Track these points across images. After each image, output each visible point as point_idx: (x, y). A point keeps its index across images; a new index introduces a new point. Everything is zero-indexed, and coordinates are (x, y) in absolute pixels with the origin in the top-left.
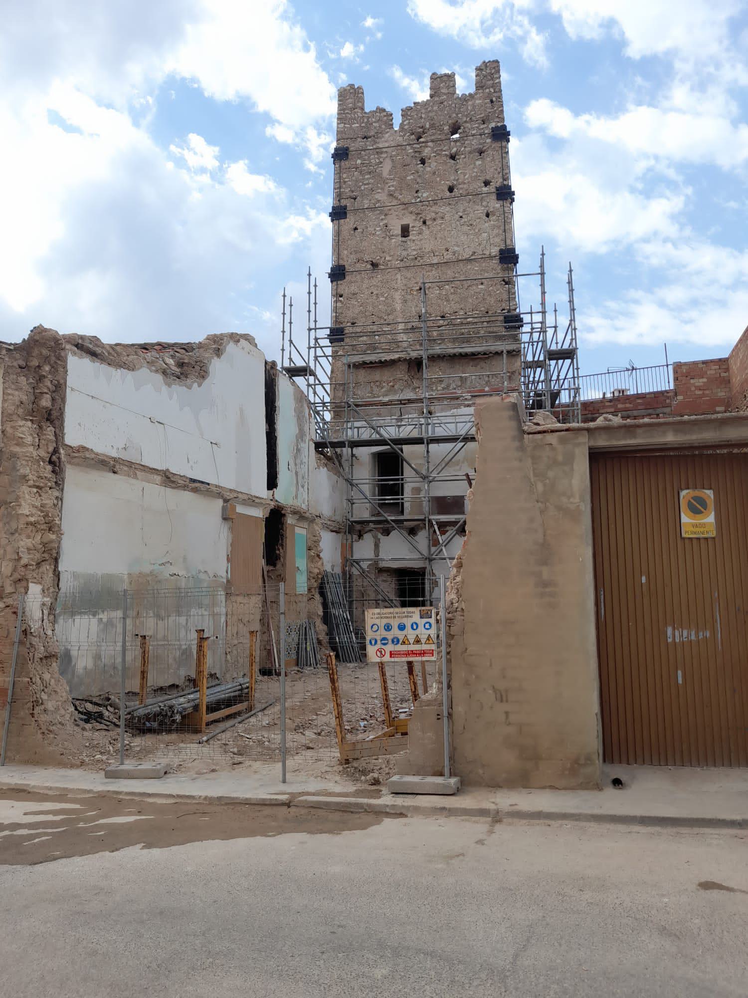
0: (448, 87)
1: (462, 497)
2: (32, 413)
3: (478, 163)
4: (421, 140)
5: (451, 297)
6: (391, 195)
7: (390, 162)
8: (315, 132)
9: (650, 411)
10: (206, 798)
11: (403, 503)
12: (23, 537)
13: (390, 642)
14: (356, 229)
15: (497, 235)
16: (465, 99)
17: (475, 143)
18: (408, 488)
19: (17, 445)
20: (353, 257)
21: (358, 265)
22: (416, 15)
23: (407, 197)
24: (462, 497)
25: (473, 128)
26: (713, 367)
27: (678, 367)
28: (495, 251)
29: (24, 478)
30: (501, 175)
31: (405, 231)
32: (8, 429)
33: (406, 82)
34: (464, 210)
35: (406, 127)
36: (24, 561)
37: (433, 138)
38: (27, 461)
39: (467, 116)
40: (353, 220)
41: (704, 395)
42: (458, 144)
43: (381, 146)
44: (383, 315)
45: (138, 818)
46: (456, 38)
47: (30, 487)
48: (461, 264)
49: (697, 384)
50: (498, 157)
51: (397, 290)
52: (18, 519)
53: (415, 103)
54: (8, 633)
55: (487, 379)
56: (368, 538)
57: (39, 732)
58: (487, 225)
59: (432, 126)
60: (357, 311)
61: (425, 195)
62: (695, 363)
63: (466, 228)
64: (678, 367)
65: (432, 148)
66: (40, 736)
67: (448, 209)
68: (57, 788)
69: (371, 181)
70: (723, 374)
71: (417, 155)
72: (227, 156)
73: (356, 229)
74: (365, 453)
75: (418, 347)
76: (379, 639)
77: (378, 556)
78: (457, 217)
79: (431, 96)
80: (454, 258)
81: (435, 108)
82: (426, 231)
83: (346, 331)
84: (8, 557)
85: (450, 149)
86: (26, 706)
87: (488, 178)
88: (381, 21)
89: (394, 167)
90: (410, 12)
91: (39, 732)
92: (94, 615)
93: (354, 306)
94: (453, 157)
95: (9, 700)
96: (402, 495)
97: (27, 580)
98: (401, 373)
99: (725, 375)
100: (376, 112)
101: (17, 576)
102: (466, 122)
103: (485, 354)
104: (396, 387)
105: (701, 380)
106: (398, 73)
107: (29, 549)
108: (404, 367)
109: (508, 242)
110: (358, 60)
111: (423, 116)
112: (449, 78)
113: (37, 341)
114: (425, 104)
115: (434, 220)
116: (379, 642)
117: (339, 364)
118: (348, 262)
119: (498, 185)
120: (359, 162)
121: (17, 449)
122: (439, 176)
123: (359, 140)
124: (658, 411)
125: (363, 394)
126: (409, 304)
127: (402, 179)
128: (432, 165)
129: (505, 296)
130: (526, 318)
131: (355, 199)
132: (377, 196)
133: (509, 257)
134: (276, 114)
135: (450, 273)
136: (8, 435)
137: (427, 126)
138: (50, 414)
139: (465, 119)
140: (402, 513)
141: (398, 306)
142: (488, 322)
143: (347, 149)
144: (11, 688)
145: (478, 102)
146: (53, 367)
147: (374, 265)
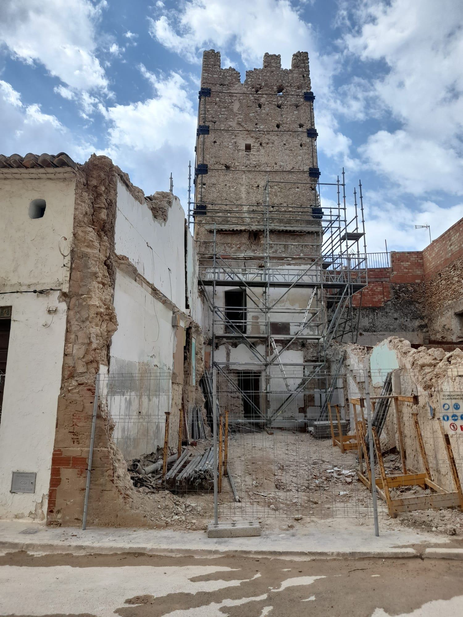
0: (276, 63)
1: (288, 324)
2: (93, 223)
3: (296, 112)
4: (259, 92)
5: (278, 194)
6: (240, 124)
7: (238, 103)
8: (88, 95)
9: (378, 280)
10: (338, 554)
11: (245, 326)
12: (93, 324)
13: (459, 418)
14: (215, 142)
15: (308, 159)
16: (286, 72)
17: (293, 100)
18: (250, 316)
19: (88, 246)
20: (213, 161)
21: (216, 166)
22: (155, 36)
23: (251, 127)
24: (288, 324)
25: (293, 91)
26: (414, 256)
27: (393, 254)
28: (306, 168)
29: (95, 275)
30: (310, 122)
31: (248, 148)
32: (80, 232)
33: (148, 75)
34: (287, 141)
35: (249, 83)
36: (94, 346)
37: (266, 92)
38: (96, 261)
39: (288, 83)
40: (213, 136)
41: (408, 272)
42: (283, 99)
43: (232, 91)
44: (234, 200)
45: (318, 577)
46: (179, 55)
47: (99, 283)
48: (285, 174)
49: (405, 265)
50: (308, 110)
51: (242, 185)
52: (89, 309)
53: (255, 69)
54: (84, 408)
55: (301, 248)
56: (222, 349)
57: (121, 497)
58: (301, 151)
59: (266, 85)
60: (215, 196)
61: (262, 127)
62: (403, 253)
63: (287, 152)
64: (394, 255)
65: (266, 99)
66: (121, 500)
67: (276, 138)
68: (179, 551)
69: (226, 113)
70: (419, 261)
71: (256, 101)
72: (27, 100)
73: (215, 142)
74: (221, 290)
75: (257, 224)
76: (450, 415)
77: (229, 361)
78: (282, 144)
79: (265, 67)
80: (280, 170)
81: (268, 74)
82: (262, 151)
83: (208, 208)
84: (80, 341)
85: (278, 101)
86: (107, 474)
87: (302, 122)
88: (137, 36)
89: (241, 106)
90: (150, 34)
91: (121, 497)
92: (123, 395)
93: (213, 192)
94: (279, 106)
95: (89, 468)
96: (246, 319)
97: (97, 362)
98: (244, 239)
99: (421, 261)
100: (229, 70)
101: (89, 358)
102: (287, 86)
103: (301, 232)
104: (242, 248)
105: (407, 263)
106: (143, 69)
107: (97, 336)
108: (247, 236)
109: (315, 164)
110: (121, 56)
111: (260, 78)
112: (277, 58)
113: (96, 165)
114: (261, 71)
115: (268, 143)
116: (450, 418)
117: (203, 229)
118: (210, 162)
119: (308, 127)
120: (218, 99)
121: (89, 250)
122: (271, 117)
123: (218, 85)
124: (383, 280)
125: (220, 251)
126: (251, 194)
127: (247, 115)
128: (266, 109)
129: (313, 197)
130: (326, 212)
131: (215, 123)
132: (230, 123)
133: (314, 173)
134: (64, 79)
135: (277, 179)
136: (79, 238)
137: (263, 85)
138: (104, 226)
139: (287, 84)
140: (245, 332)
141: (244, 196)
142: (302, 212)
143: (210, 90)
144: (90, 457)
145: (295, 75)
146: (106, 188)
147: (227, 167)
